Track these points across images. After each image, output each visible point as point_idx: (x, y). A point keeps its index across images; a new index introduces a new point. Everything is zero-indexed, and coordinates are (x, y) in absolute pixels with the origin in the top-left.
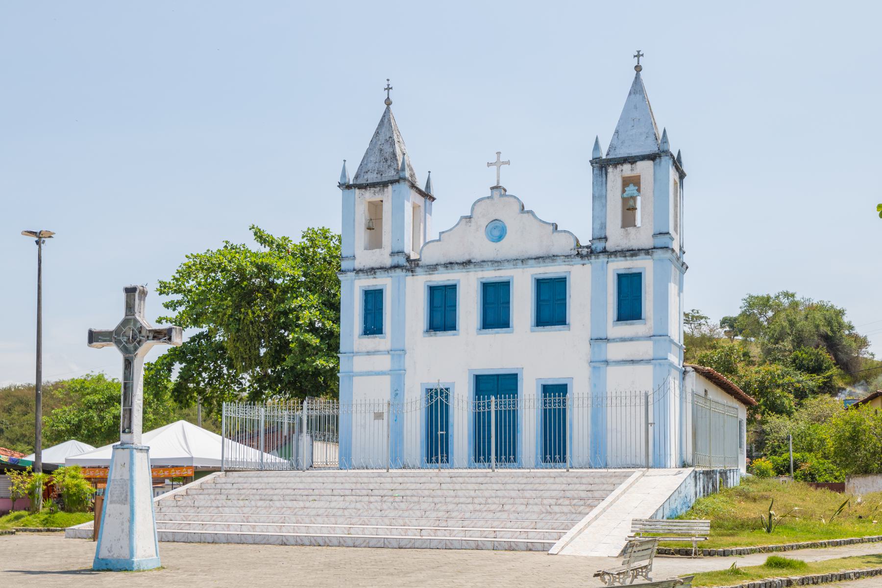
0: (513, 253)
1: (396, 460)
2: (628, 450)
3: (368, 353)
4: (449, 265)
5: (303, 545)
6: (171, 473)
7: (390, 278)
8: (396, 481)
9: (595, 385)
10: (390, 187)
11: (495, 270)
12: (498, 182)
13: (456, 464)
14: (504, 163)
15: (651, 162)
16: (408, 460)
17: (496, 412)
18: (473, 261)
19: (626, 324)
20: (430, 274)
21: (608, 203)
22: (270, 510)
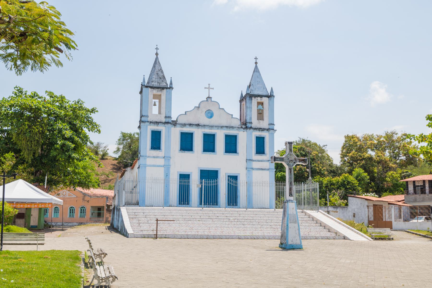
0: (216, 124)
1: (167, 203)
2: (128, 198)
3: (154, 157)
4: (190, 125)
5: (248, 239)
6: (39, 206)
7: (164, 127)
9: (248, 177)
10: (165, 90)
11: (209, 129)
12: (209, 95)
13: (193, 205)
14: (211, 88)
15: (267, 98)
16: (171, 203)
17: (205, 186)
18: (200, 124)
19: (260, 155)
20: (182, 127)
21: (252, 110)
22: (195, 225)
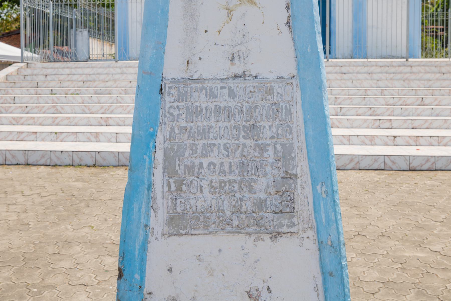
8: (63, 73)
